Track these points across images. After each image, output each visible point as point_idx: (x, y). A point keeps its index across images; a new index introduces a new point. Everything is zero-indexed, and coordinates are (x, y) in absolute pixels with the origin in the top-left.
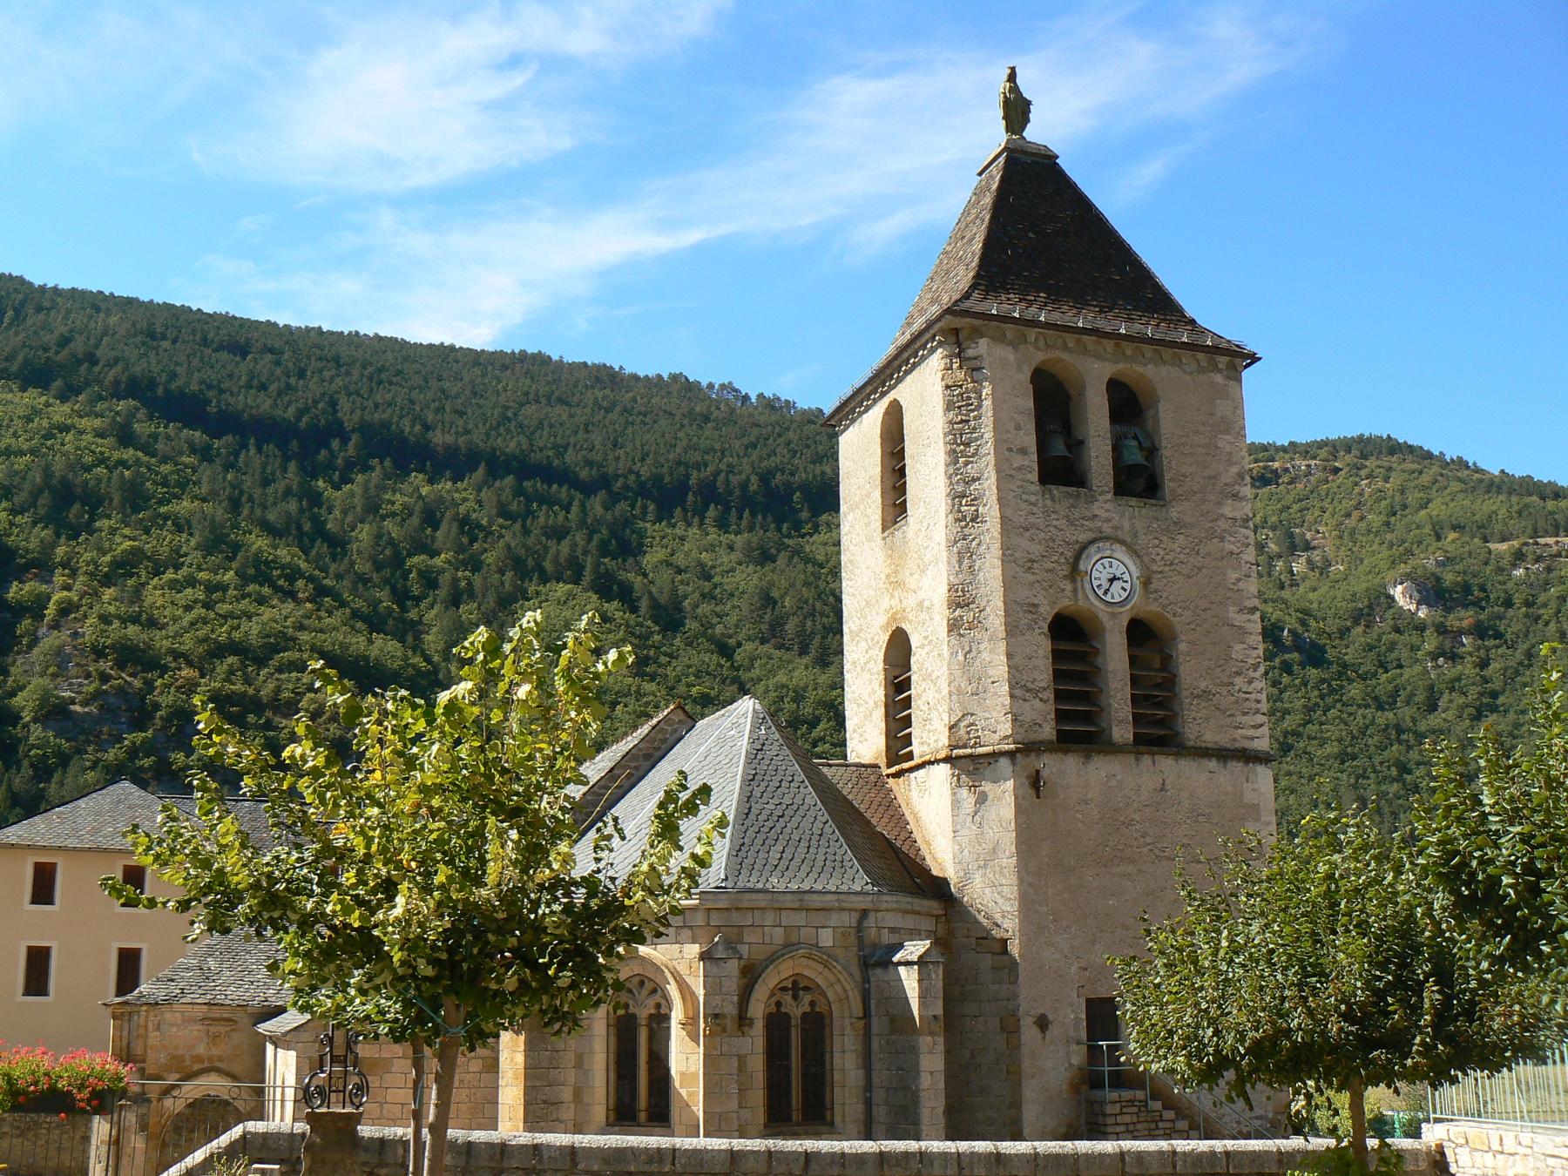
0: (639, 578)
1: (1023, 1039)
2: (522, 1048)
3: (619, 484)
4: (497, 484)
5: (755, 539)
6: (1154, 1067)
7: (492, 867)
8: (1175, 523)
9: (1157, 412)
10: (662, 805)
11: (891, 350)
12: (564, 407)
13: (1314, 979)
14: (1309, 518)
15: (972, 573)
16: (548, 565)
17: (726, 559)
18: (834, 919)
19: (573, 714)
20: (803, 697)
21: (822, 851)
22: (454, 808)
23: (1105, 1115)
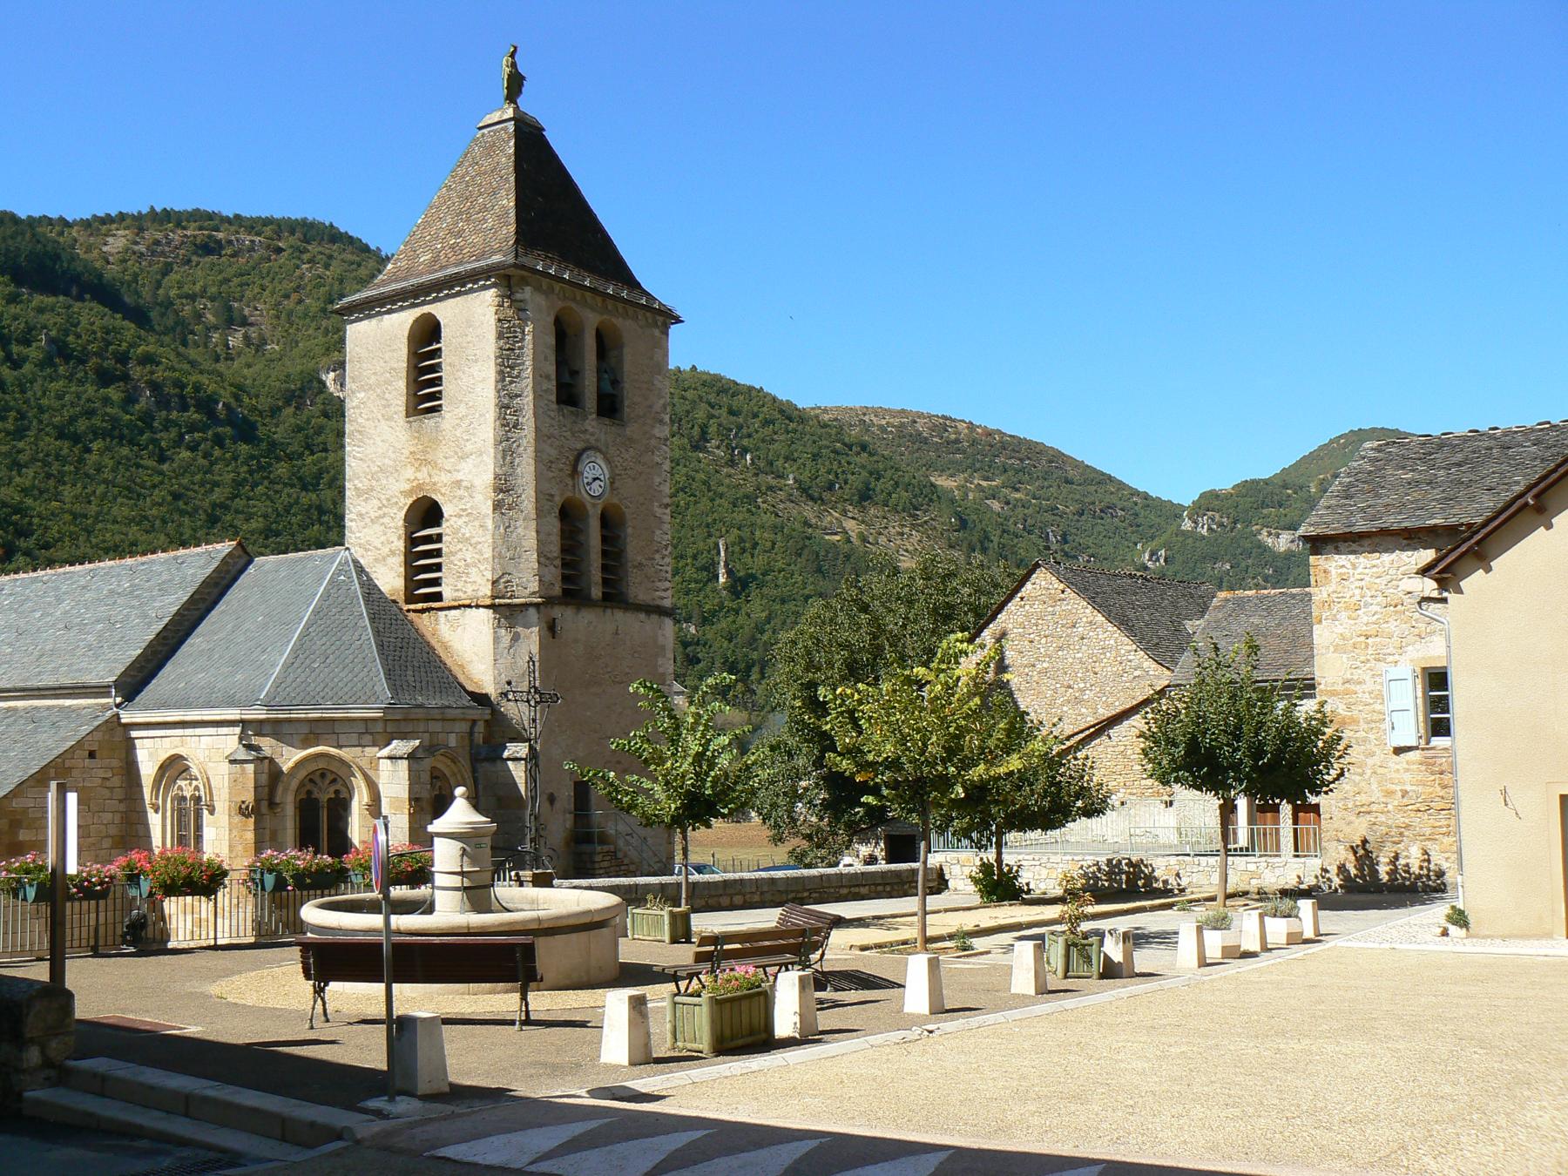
14: (248, 294)
15: (512, 467)
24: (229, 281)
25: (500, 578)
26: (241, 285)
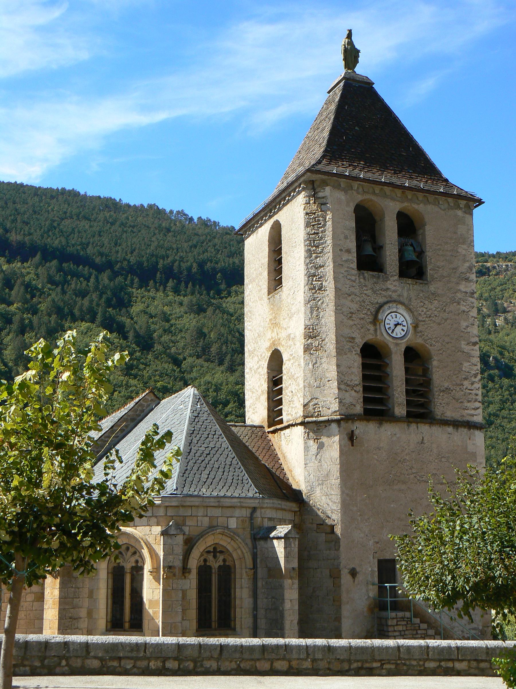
0: (129, 320)
1: (343, 581)
2: (58, 586)
3: (118, 266)
4: (48, 264)
5: (194, 300)
6: (418, 597)
7: (46, 477)
8: (433, 294)
9: (424, 231)
10: (143, 443)
11: (274, 192)
12: (87, 221)
13: (508, 549)
14: (506, 295)
16: (76, 312)
17: (178, 310)
18: (237, 513)
19: (94, 390)
20: (220, 389)
21: (231, 474)
22: (24, 444)
23: (387, 626)
24: (495, 289)
25: (309, 401)
26: (502, 291)
